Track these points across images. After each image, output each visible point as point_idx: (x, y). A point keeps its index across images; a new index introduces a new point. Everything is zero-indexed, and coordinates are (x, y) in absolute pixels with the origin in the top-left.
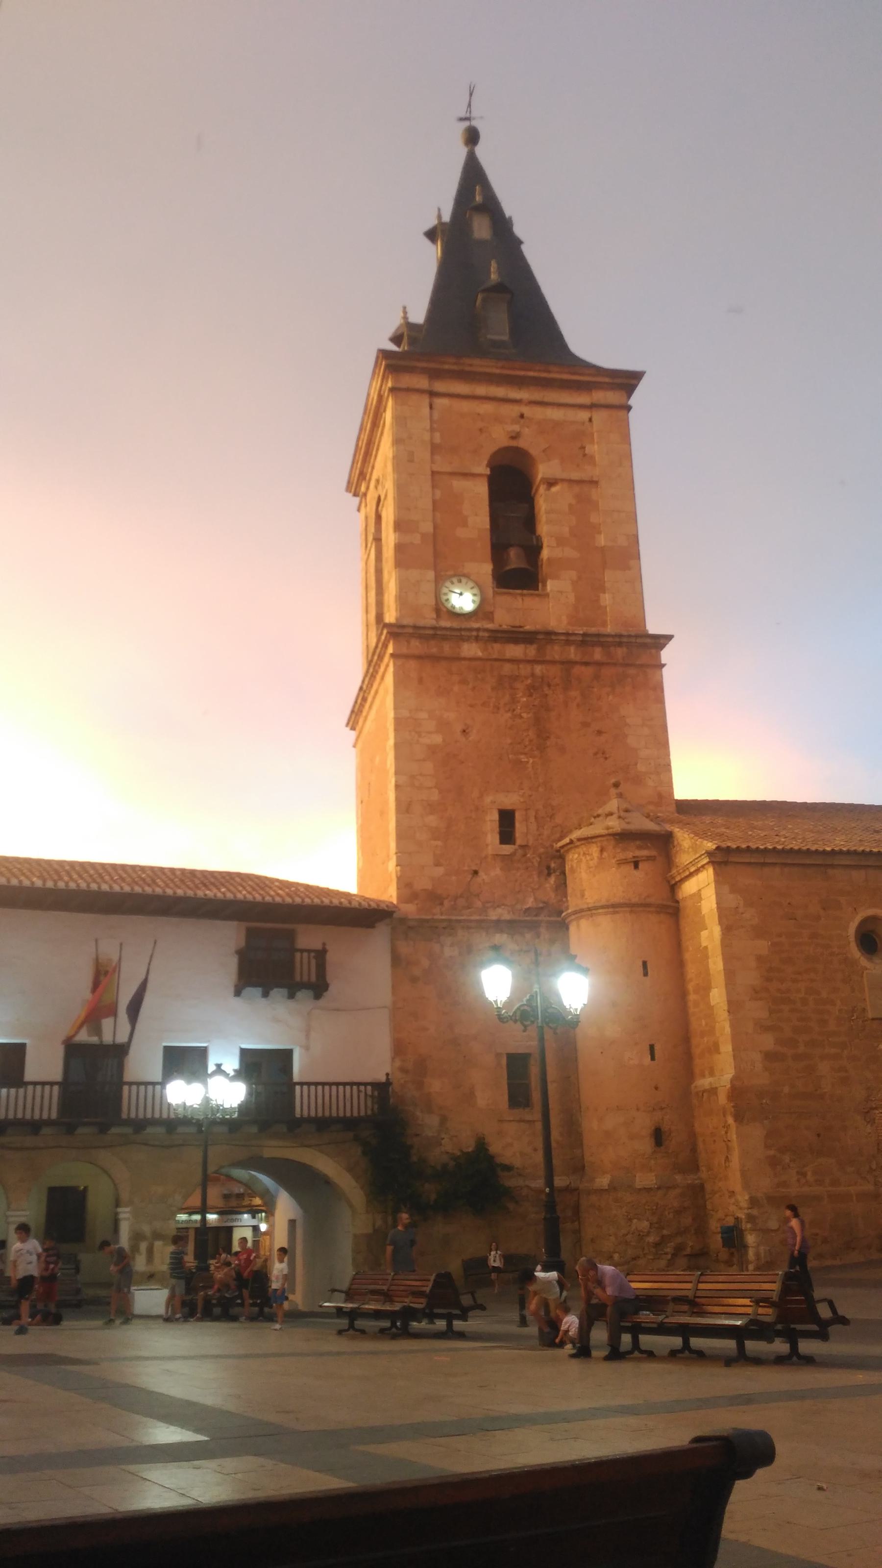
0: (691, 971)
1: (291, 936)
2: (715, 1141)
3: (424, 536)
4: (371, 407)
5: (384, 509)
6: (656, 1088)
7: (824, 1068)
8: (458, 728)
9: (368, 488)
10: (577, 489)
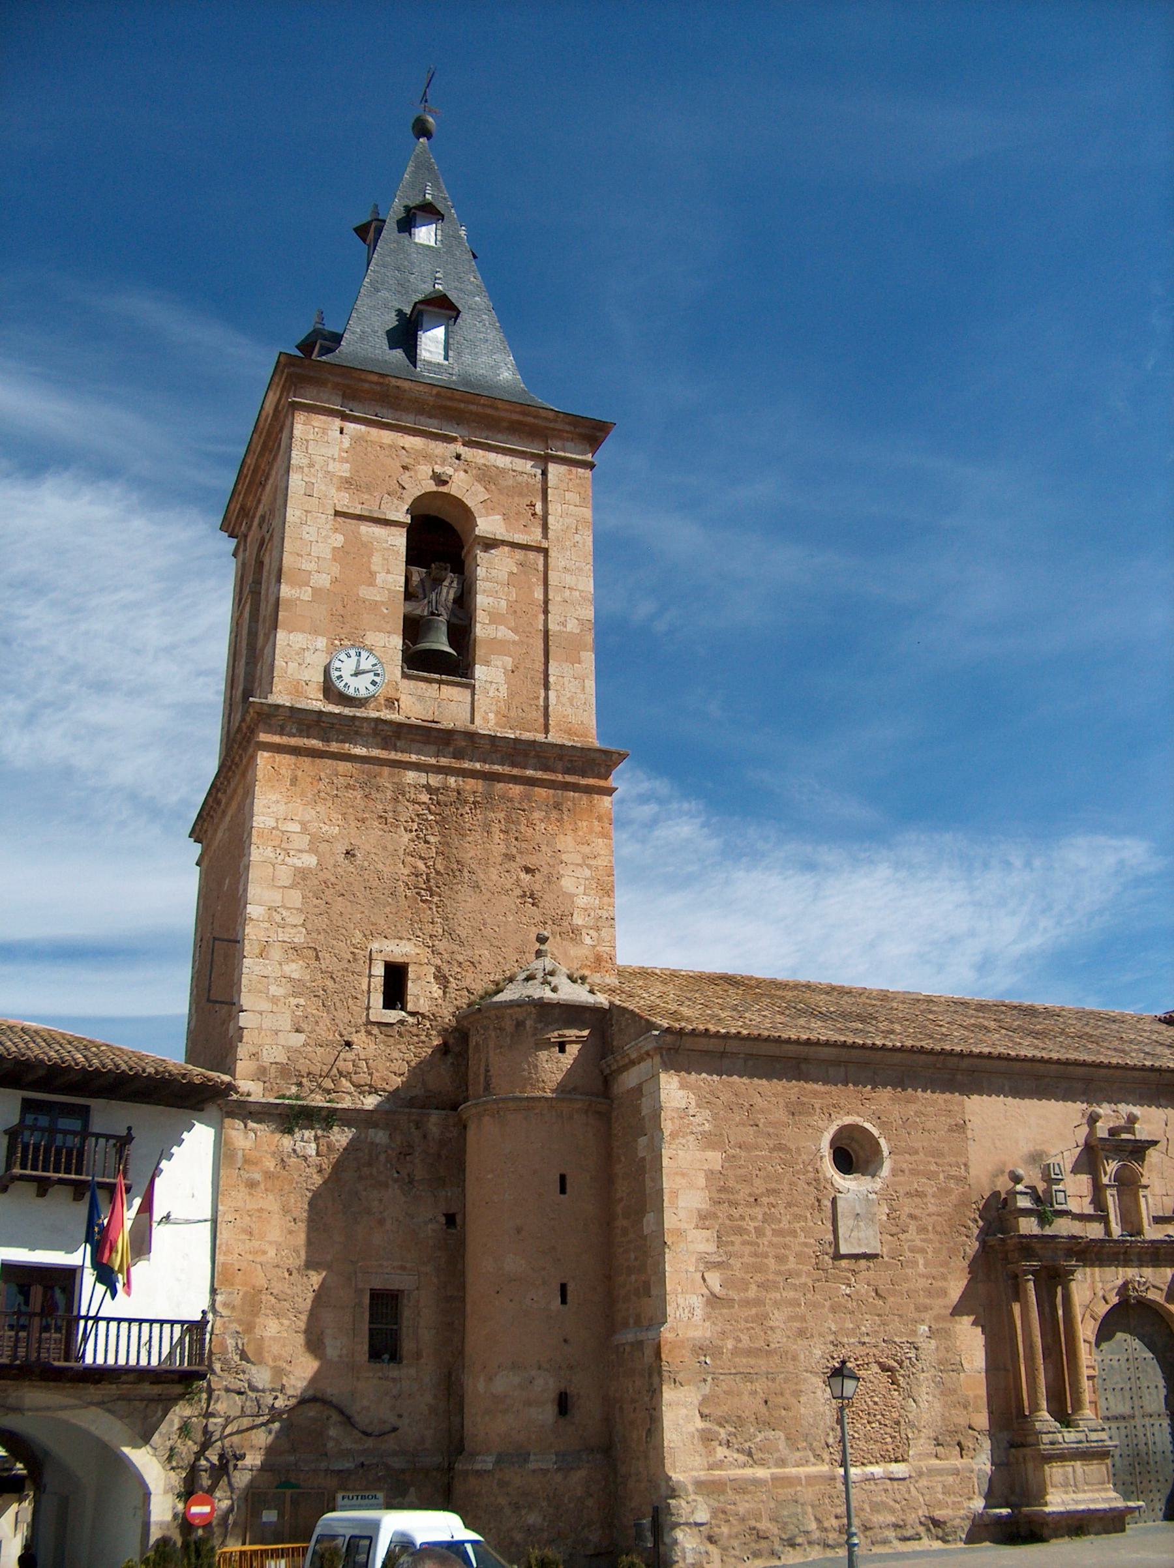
0: (622, 1189)
1: (84, 1113)
2: (635, 1409)
3: (316, 591)
4: (264, 425)
5: (267, 554)
6: (565, 1341)
7: (778, 1318)
8: (341, 848)
9: (250, 528)
10: (519, 554)
